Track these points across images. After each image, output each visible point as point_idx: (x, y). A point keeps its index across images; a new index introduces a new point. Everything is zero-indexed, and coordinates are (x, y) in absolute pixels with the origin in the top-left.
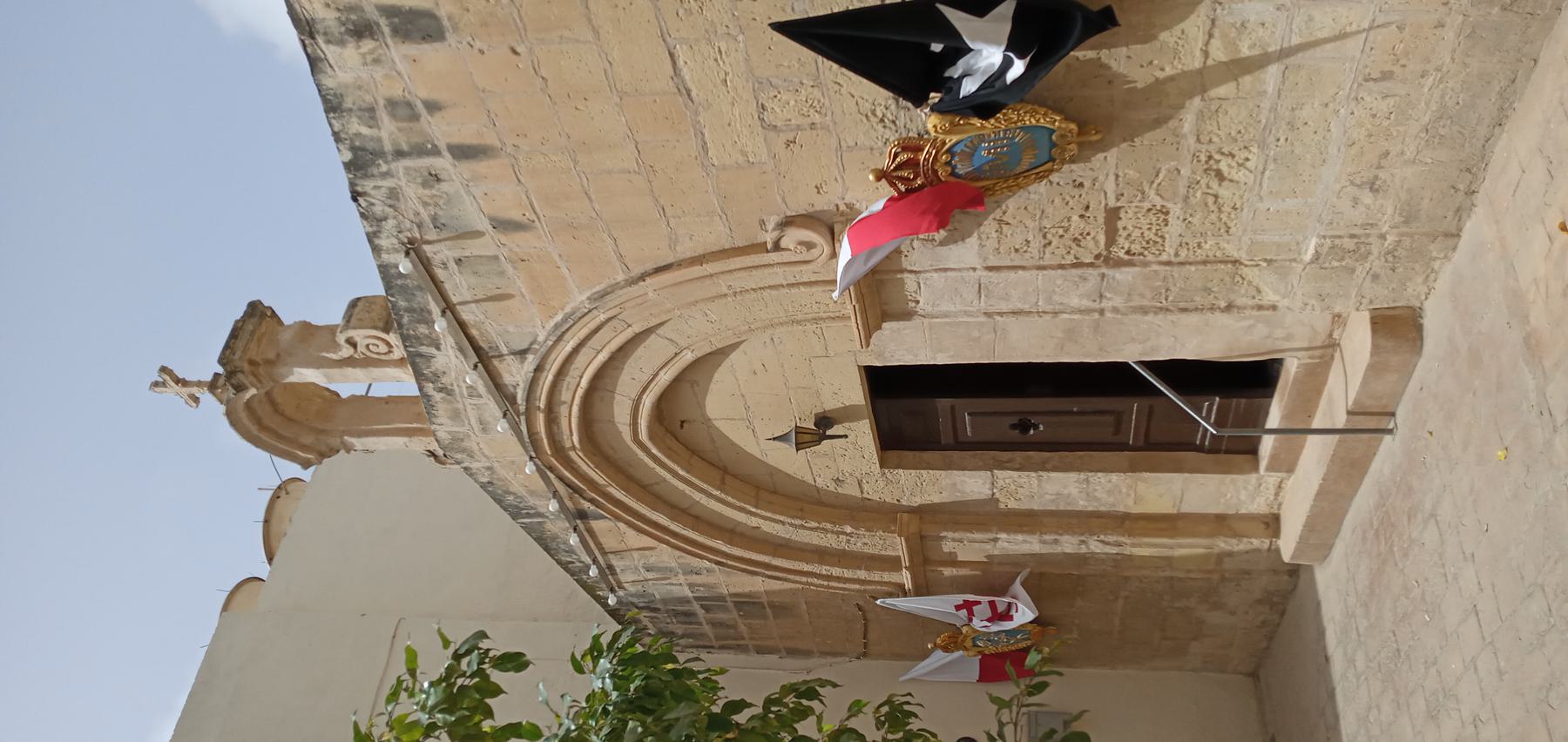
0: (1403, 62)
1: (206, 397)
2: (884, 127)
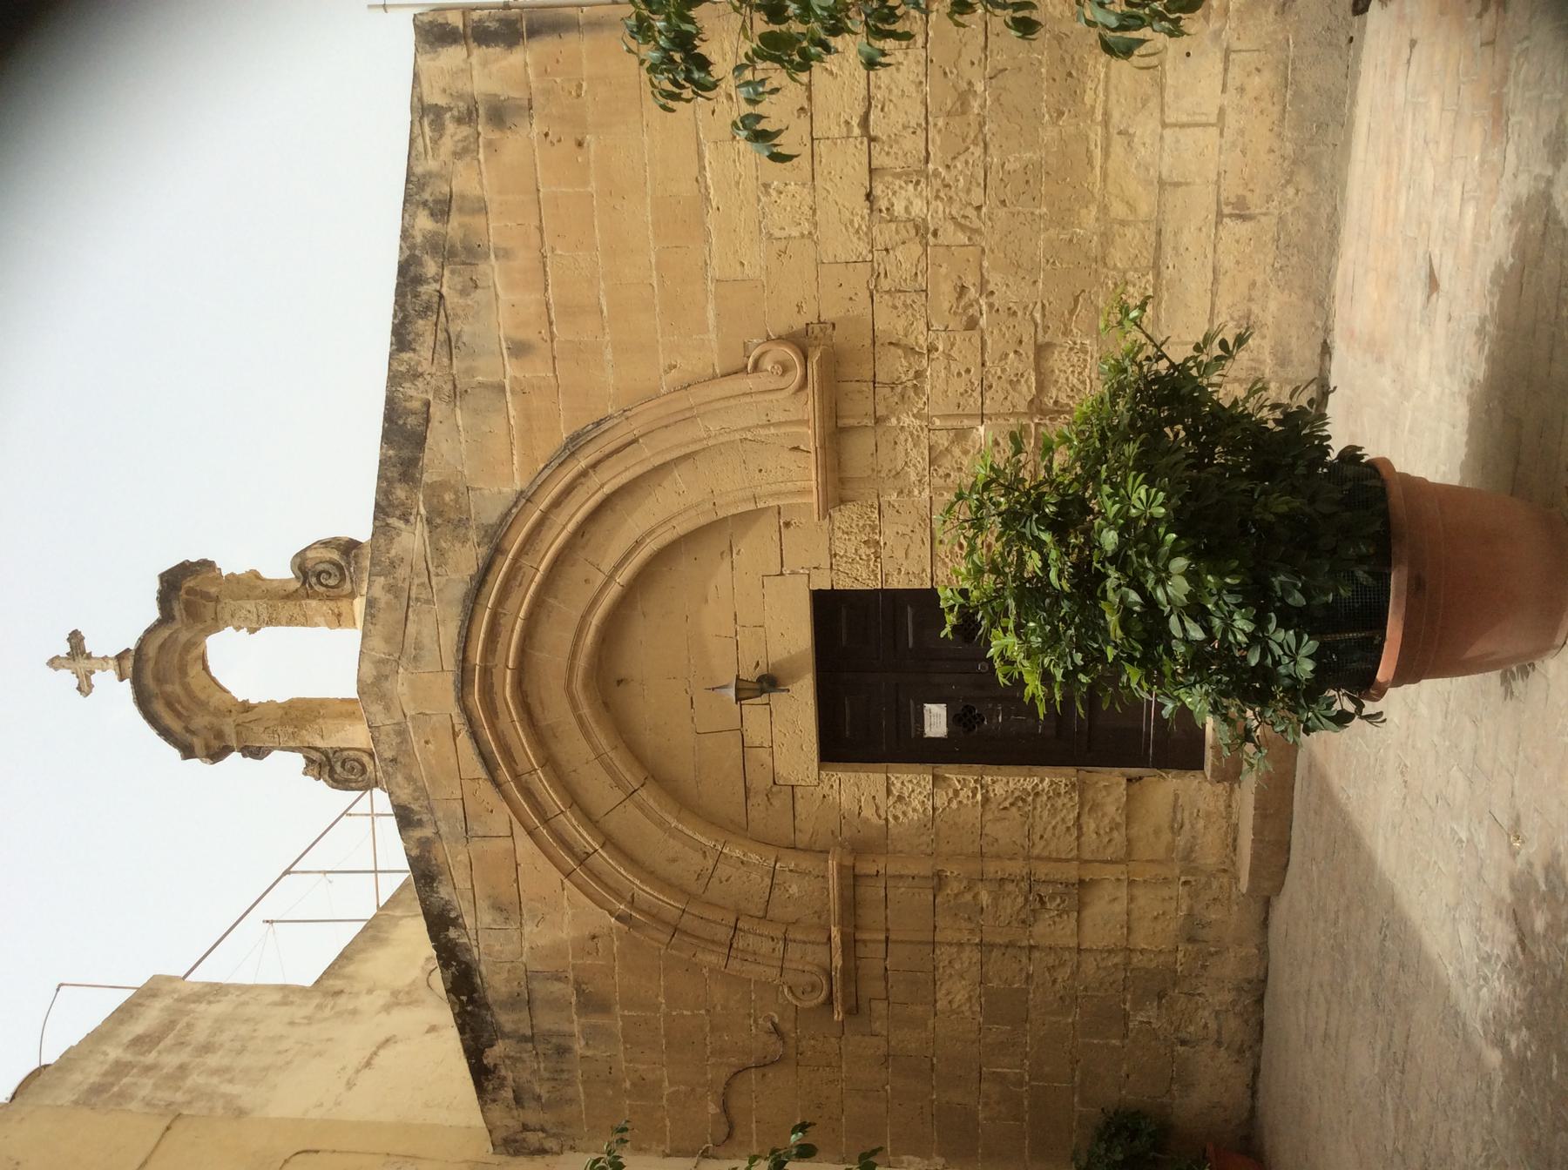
2: (859, 239)
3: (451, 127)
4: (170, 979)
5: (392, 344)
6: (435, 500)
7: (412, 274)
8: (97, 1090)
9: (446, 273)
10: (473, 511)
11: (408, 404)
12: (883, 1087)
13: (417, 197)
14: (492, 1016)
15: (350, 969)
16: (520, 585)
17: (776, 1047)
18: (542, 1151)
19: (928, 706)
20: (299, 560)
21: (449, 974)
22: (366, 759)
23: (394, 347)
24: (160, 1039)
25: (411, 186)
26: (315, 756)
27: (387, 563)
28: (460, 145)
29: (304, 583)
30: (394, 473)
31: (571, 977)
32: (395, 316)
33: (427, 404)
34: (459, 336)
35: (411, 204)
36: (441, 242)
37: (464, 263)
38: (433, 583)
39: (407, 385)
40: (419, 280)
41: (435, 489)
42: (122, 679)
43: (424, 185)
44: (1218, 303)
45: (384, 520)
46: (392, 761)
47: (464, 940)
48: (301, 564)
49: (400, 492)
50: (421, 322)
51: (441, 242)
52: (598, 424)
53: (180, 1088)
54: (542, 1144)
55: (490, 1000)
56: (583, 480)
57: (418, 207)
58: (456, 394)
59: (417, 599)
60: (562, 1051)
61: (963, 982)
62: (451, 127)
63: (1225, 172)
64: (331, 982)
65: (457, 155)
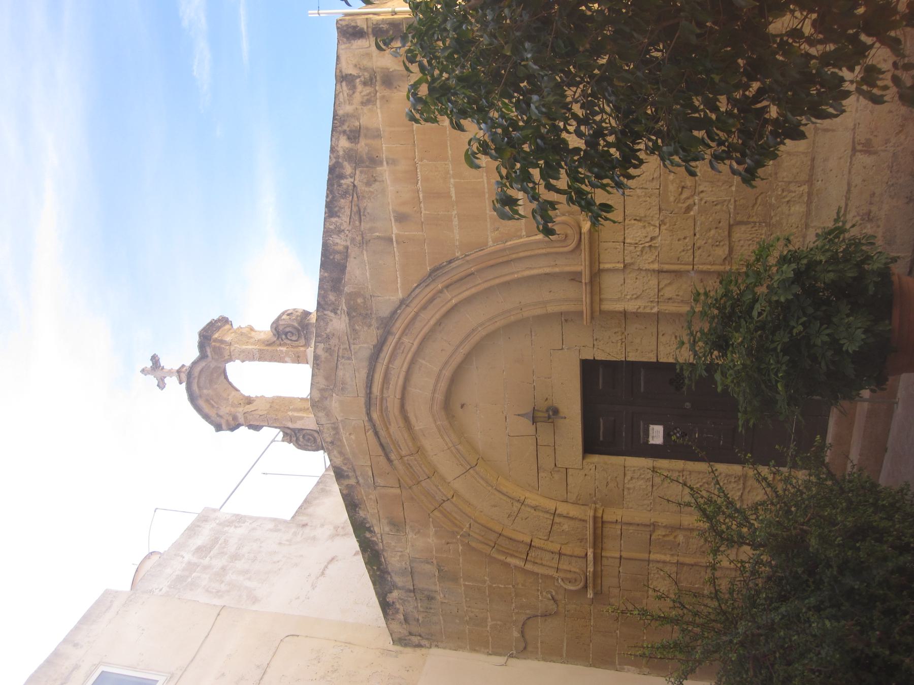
0: (875, 133)
1: (172, 382)
3: (360, 87)
4: (214, 510)
5: (325, 213)
6: (352, 302)
7: (337, 173)
8: (180, 579)
9: (357, 172)
10: (374, 309)
11: (336, 247)
12: (615, 631)
13: (340, 128)
14: (391, 578)
15: (310, 510)
16: (403, 352)
17: (552, 606)
18: (419, 646)
19: (651, 427)
20: (275, 325)
21: (366, 556)
22: (316, 435)
23: (327, 215)
24: (211, 549)
25: (336, 122)
26: (289, 431)
27: (325, 336)
28: (366, 98)
29: (278, 338)
30: (327, 286)
31: (435, 562)
32: (327, 197)
33: (347, 248)
34: (365, 209)
35: (337, 132)
36: (354, 155)
37: (367, 167)
38: (352, 348)
39: (335, 236)
40: (341, 176)
41: (352, 296)
42: (181, 383)
43: (344, 120)
44: (850, 204)
45: (323, 312)
46: (331, 443)
47: (375, 539)
48: (276, 326)
49: (332, 297)
50: (342, 200)
51: (354, 155)
52: (450, 262)
53: (223, 582)
54: (419, 643)
55: (390, 570)
56: (440, 295)
57: (340, 134)
58: (364, 243)
59: (343, 357)
60: (430, 598)
61: (665, 582)
62: (360, 87)
63: (859, 124)
64: (300, 518)
65: (363, 104)
